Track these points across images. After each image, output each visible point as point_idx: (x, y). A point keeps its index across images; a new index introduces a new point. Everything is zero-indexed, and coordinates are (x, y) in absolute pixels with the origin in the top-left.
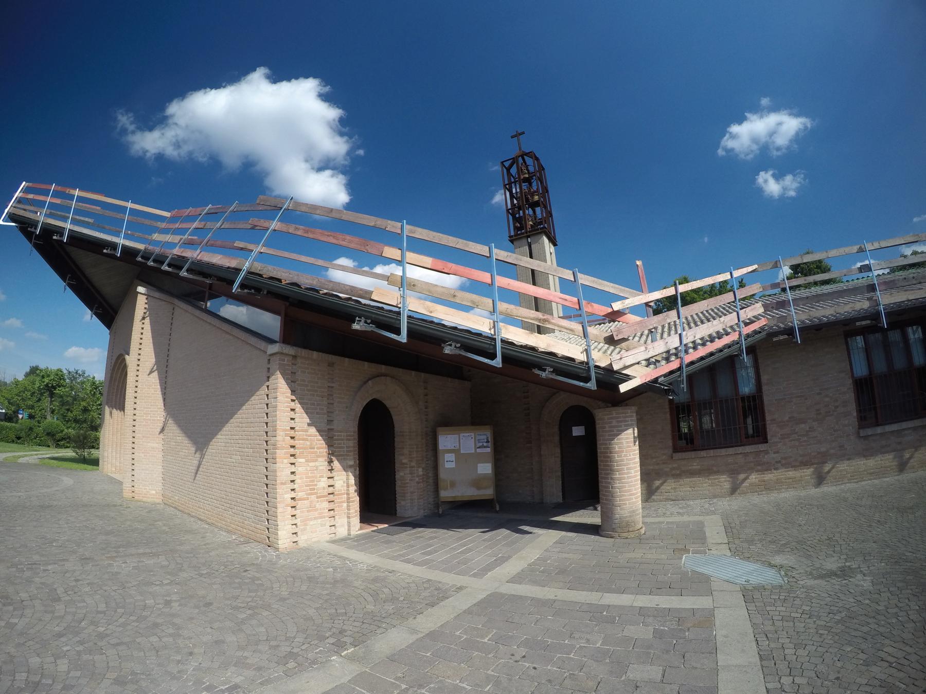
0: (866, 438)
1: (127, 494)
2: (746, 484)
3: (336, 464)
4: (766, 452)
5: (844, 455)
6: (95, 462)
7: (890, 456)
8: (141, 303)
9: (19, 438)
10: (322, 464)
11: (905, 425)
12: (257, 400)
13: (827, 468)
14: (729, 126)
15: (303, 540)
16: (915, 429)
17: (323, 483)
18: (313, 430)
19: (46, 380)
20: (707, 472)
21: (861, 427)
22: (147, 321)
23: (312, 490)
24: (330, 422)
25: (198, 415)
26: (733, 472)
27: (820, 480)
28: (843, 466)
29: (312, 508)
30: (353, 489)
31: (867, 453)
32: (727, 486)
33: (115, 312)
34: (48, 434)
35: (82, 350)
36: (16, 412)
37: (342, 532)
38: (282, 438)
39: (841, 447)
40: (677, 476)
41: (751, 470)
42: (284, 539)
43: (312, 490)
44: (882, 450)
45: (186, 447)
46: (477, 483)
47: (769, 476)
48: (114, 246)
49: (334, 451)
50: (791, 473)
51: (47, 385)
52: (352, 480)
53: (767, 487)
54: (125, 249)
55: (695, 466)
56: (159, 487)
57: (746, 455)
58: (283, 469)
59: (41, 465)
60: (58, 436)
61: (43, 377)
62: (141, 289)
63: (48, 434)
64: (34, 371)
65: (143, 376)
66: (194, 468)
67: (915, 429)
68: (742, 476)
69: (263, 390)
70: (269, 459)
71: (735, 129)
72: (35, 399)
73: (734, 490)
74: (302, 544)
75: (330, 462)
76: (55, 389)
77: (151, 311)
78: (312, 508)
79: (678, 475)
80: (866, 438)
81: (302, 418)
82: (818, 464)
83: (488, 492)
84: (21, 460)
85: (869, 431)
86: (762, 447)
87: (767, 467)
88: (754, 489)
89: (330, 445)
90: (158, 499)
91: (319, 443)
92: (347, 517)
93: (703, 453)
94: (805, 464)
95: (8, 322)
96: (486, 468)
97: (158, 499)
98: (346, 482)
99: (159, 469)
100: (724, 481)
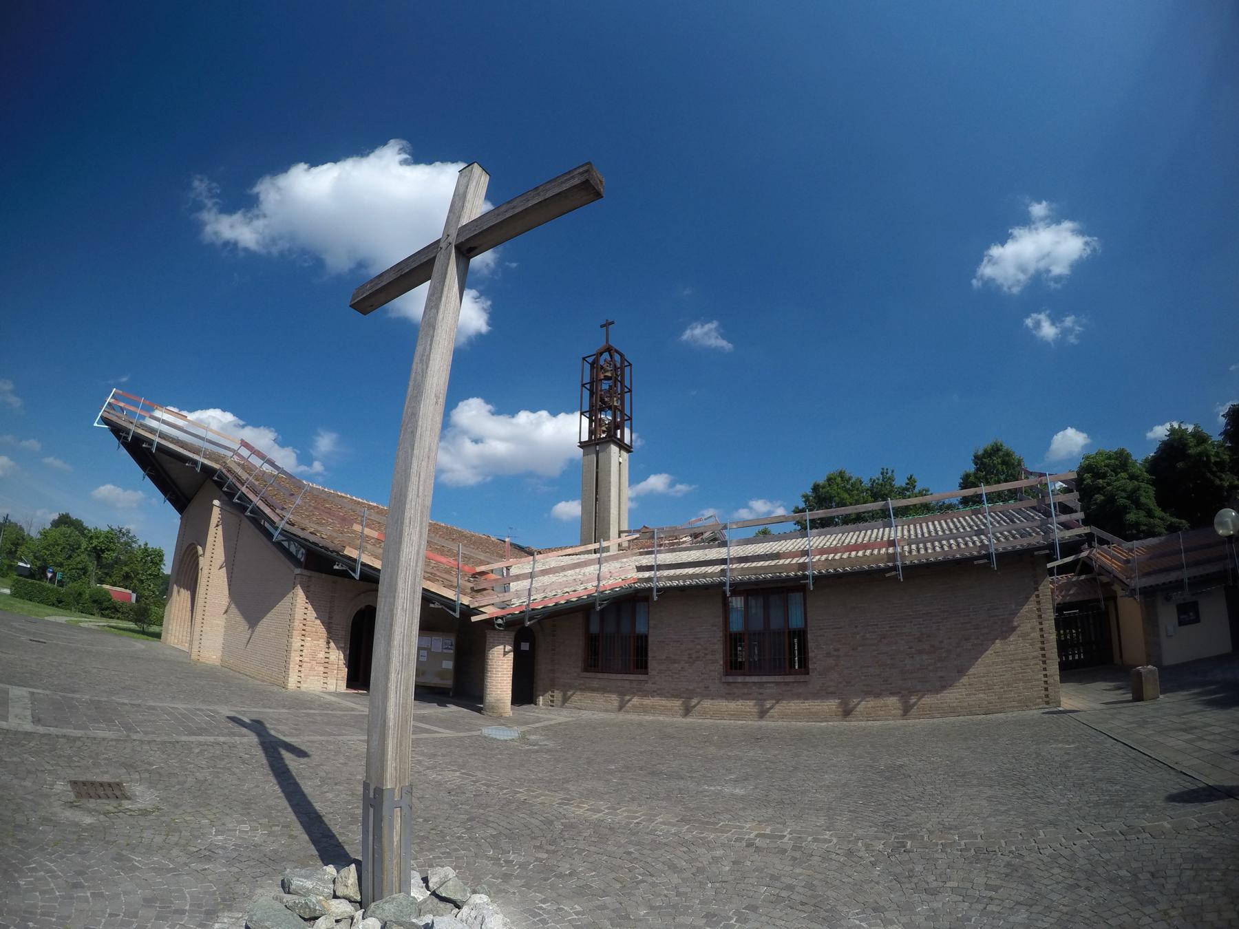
0: (729, 683)
1: (194, 657)
2: (629, 705)
3: (332, 644)
4: (646, 682)
5: (707, 694)
6: (158, 636)
7: (752, 703)
8: (216, 514)
9: (60, 602)
10: (322, 643)
11: (765, 679)
12: (286, 601)
13: (694, 702)
14: (988, 247)
15: (304, 687)
16: (777, 683)
17: (322, 655)
18: (318, 622)
19: (95, 542)
20: (603, 690)
21: (727, 674)
22: (220, 528)
23: (314, 658)
24: (330, 618)
25: (251, 602)
26: (621, 694)
27: (687, 711)
28: (707, 703)
29: (312, 669)
30: (342, 662)
31: (729, 696)
32: (616, 704)
33: (189, 500)
34: (95, 601)
35: (119, 490)
36: (43, 570)
37: (332, 688)
38: (297, 624)
39: (707, 688)
40: (582, 690)
41: (634, 694)
42: (292, 683)
43: (314, 658)
44: (745, 696)
45: (243, 625)
46: (442, 674)
47: (647, 701)
48: (195, 462)
49: (332, 636)
50: (664, 702)
51: (95, 548)
52: (342, 656)
53: (645, 710)
54: (204, 467)
55: (595, 684)
56: (219, 654)
57: (631, 681)
58: (296, 642)
59: (102, 630)
60: (106, 604)
61: (91, 538)
62: (216, 502)
63: (95, 601)
64: (64, 520)
65: (215, 570)
66: (245, 641)
67: (777, 683)
68: (627, 698)
69: (290, 595)
70: (290, 636)
71: (996, 251)
72: (64, 555)
73: (621, 708)
74: (303, 689)
75: (328, 643)
76: (103, 551)
77: (224, 522)
78: (312, 669)
79: (584, 689)
80: (729, 683)
81: (312, 614)
82: (687, 698)
83: (449, 683)
84: (82, 625)
85: (731, 679)
86: (642, 677)
87: (646, 694)
88: (635, 710)
89: (329, 632)
90: (218, 663)
91: (322, 631)
92: (342, 687)
93: (600, 675)
94: (674, 695)
95: (25, 443)
96: (448, 665)
97: (218, 663)
98: (337, 657)
99: (221, 640)
100: (614, 699)
